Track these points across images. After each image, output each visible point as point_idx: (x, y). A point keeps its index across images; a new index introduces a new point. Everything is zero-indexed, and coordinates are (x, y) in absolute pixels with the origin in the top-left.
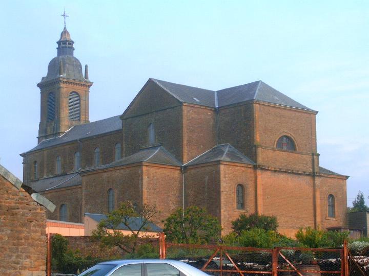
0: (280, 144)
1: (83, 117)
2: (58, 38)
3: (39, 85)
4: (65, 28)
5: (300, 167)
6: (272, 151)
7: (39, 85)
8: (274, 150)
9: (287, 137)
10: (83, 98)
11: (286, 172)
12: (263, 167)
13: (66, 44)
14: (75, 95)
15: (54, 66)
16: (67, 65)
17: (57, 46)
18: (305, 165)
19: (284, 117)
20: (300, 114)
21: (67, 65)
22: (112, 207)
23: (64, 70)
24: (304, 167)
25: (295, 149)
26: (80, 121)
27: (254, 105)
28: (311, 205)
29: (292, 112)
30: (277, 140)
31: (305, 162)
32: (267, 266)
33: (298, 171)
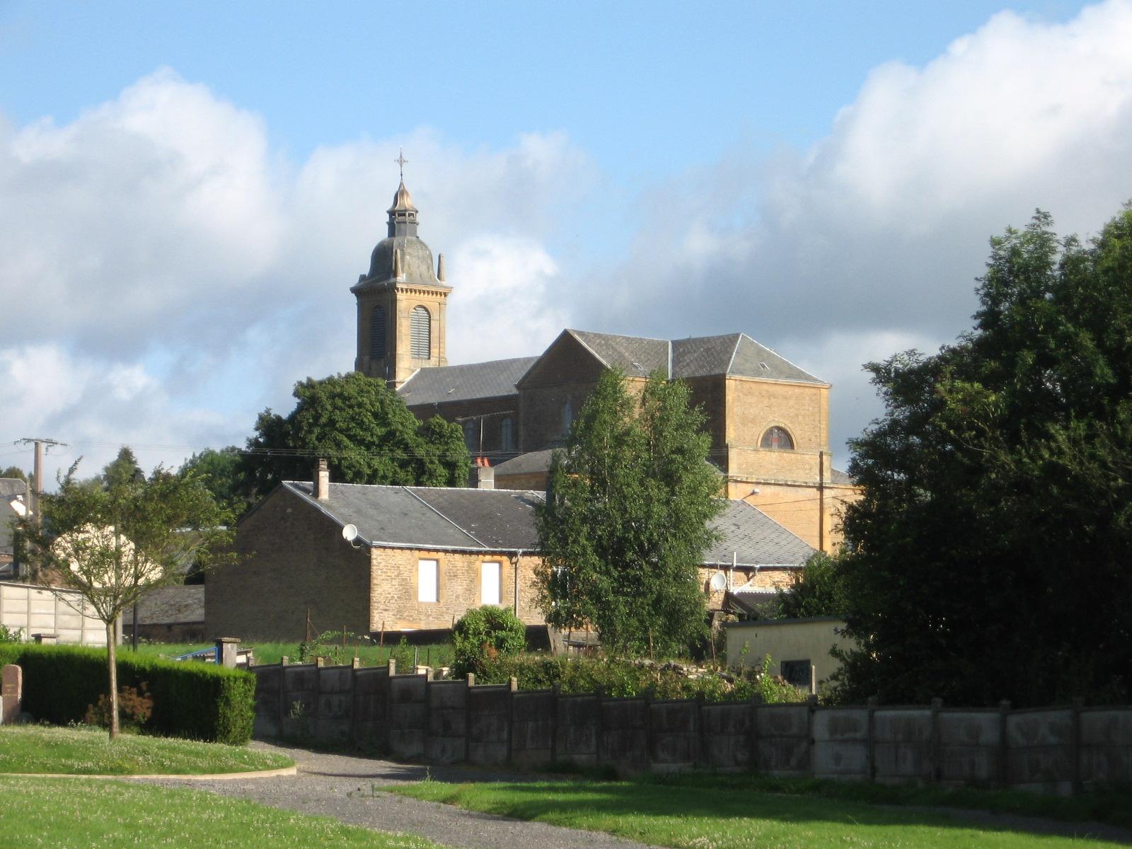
0: (767, 441)
1: (434, 351)
2: (389, 205)
3: (354, 290)
4: (401, 184)
5: (801, 477)
6: (754, 452)
7: (354, 290)
8: (756, 450)
9: (779, 428)
10: (435, 316)
11: (775, 484)
12: (738, 479)
13: (404, 215)
14: (421, 311)
15: (384, 260)
16: (408, 257)
17: (387, 218)
18: (807, 472)
19: (775, 398)
20: (801, 390)
21: (408, 257)
22: (972, 836)
23: (403, 266)
24: (807, 474)
25: (792, 446)
26: (429, 358)
27: (727, 381)
28: (817, 533)
29: (787, 389)
30: (762, 435)
31: (807, 466)
32: (1071, 532)
33: (794, 481)
